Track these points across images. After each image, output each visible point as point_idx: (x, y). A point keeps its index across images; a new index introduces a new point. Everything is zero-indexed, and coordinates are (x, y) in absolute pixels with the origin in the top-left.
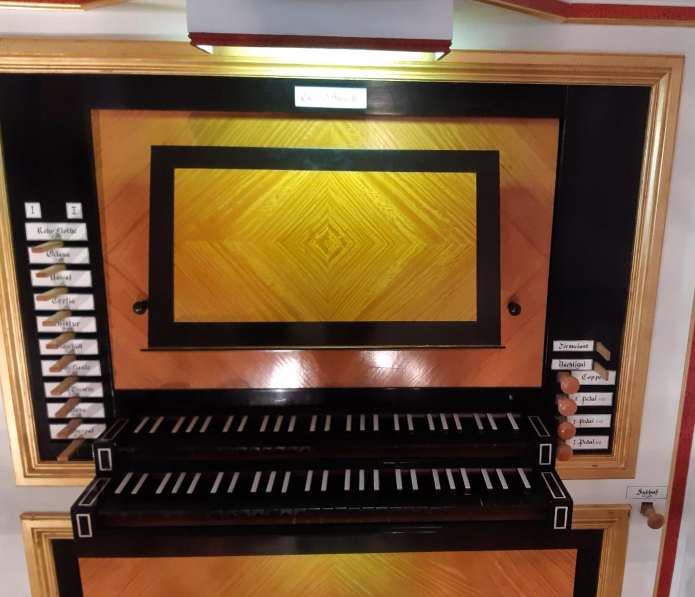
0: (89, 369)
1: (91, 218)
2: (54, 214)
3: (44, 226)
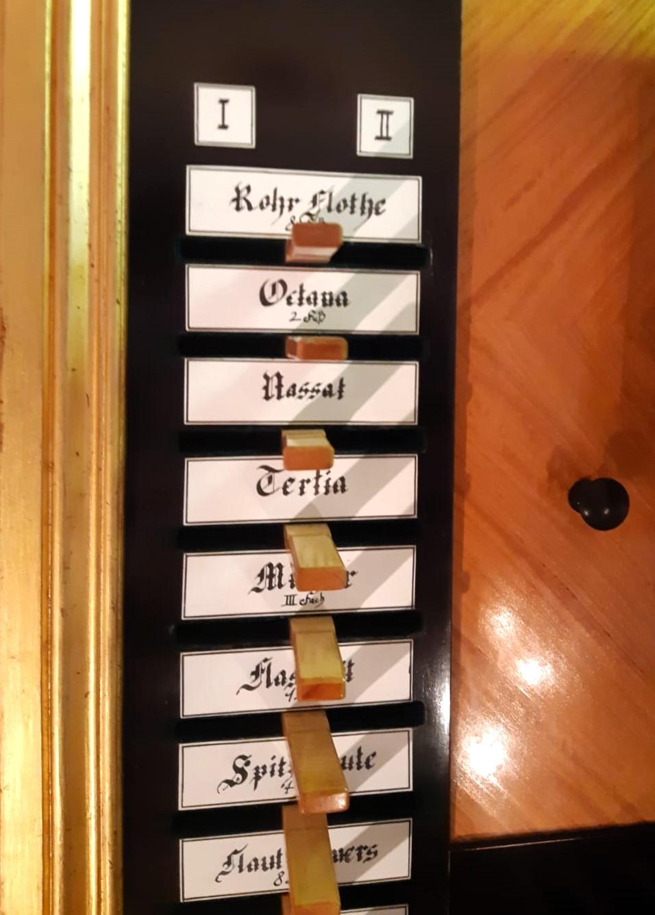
1: (435, 159)
2: (303, 133)
3: (262, 181)
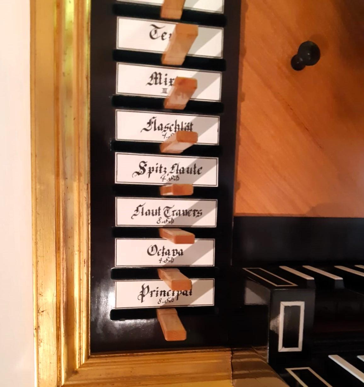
0: (199, 173)
